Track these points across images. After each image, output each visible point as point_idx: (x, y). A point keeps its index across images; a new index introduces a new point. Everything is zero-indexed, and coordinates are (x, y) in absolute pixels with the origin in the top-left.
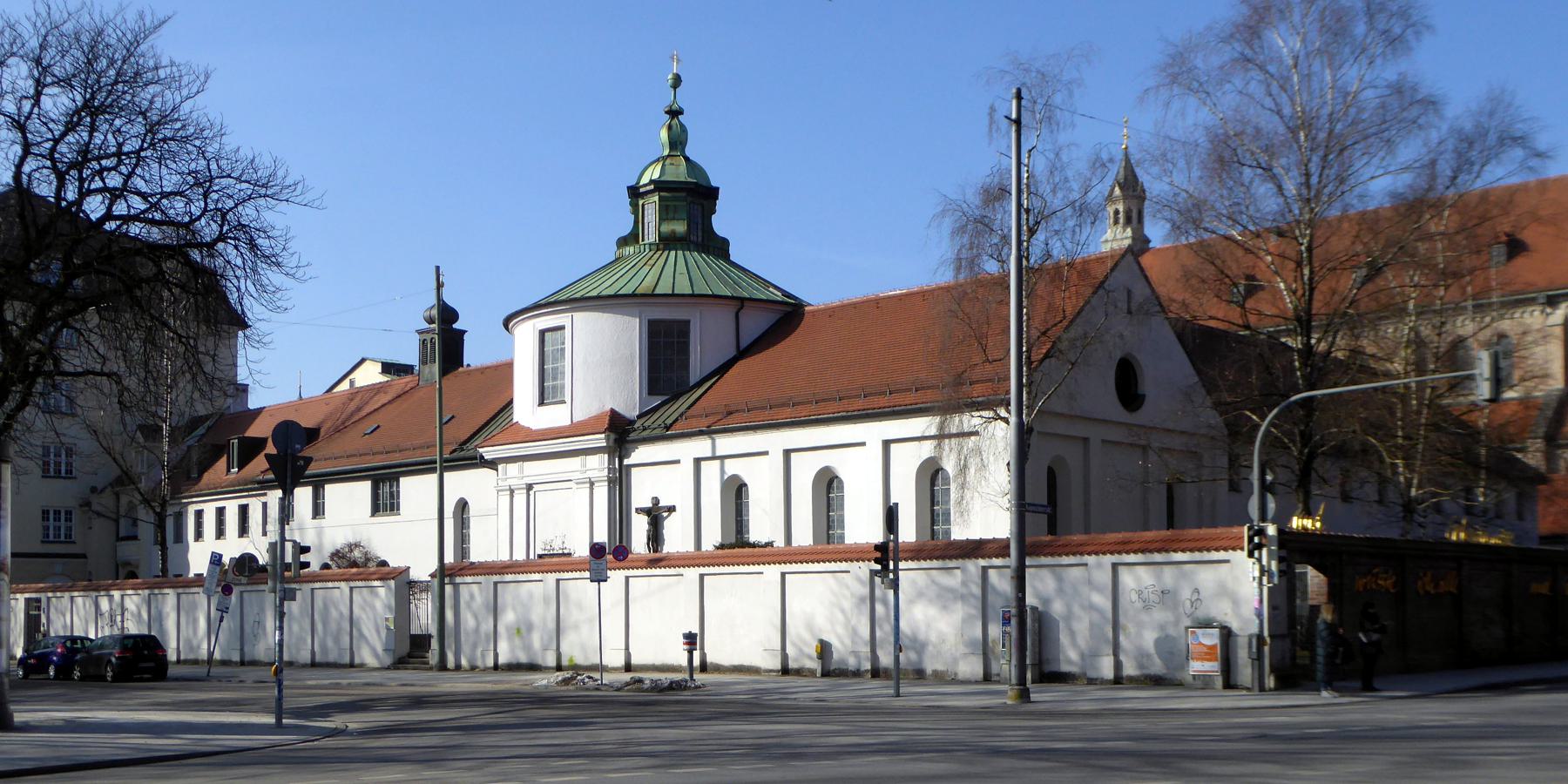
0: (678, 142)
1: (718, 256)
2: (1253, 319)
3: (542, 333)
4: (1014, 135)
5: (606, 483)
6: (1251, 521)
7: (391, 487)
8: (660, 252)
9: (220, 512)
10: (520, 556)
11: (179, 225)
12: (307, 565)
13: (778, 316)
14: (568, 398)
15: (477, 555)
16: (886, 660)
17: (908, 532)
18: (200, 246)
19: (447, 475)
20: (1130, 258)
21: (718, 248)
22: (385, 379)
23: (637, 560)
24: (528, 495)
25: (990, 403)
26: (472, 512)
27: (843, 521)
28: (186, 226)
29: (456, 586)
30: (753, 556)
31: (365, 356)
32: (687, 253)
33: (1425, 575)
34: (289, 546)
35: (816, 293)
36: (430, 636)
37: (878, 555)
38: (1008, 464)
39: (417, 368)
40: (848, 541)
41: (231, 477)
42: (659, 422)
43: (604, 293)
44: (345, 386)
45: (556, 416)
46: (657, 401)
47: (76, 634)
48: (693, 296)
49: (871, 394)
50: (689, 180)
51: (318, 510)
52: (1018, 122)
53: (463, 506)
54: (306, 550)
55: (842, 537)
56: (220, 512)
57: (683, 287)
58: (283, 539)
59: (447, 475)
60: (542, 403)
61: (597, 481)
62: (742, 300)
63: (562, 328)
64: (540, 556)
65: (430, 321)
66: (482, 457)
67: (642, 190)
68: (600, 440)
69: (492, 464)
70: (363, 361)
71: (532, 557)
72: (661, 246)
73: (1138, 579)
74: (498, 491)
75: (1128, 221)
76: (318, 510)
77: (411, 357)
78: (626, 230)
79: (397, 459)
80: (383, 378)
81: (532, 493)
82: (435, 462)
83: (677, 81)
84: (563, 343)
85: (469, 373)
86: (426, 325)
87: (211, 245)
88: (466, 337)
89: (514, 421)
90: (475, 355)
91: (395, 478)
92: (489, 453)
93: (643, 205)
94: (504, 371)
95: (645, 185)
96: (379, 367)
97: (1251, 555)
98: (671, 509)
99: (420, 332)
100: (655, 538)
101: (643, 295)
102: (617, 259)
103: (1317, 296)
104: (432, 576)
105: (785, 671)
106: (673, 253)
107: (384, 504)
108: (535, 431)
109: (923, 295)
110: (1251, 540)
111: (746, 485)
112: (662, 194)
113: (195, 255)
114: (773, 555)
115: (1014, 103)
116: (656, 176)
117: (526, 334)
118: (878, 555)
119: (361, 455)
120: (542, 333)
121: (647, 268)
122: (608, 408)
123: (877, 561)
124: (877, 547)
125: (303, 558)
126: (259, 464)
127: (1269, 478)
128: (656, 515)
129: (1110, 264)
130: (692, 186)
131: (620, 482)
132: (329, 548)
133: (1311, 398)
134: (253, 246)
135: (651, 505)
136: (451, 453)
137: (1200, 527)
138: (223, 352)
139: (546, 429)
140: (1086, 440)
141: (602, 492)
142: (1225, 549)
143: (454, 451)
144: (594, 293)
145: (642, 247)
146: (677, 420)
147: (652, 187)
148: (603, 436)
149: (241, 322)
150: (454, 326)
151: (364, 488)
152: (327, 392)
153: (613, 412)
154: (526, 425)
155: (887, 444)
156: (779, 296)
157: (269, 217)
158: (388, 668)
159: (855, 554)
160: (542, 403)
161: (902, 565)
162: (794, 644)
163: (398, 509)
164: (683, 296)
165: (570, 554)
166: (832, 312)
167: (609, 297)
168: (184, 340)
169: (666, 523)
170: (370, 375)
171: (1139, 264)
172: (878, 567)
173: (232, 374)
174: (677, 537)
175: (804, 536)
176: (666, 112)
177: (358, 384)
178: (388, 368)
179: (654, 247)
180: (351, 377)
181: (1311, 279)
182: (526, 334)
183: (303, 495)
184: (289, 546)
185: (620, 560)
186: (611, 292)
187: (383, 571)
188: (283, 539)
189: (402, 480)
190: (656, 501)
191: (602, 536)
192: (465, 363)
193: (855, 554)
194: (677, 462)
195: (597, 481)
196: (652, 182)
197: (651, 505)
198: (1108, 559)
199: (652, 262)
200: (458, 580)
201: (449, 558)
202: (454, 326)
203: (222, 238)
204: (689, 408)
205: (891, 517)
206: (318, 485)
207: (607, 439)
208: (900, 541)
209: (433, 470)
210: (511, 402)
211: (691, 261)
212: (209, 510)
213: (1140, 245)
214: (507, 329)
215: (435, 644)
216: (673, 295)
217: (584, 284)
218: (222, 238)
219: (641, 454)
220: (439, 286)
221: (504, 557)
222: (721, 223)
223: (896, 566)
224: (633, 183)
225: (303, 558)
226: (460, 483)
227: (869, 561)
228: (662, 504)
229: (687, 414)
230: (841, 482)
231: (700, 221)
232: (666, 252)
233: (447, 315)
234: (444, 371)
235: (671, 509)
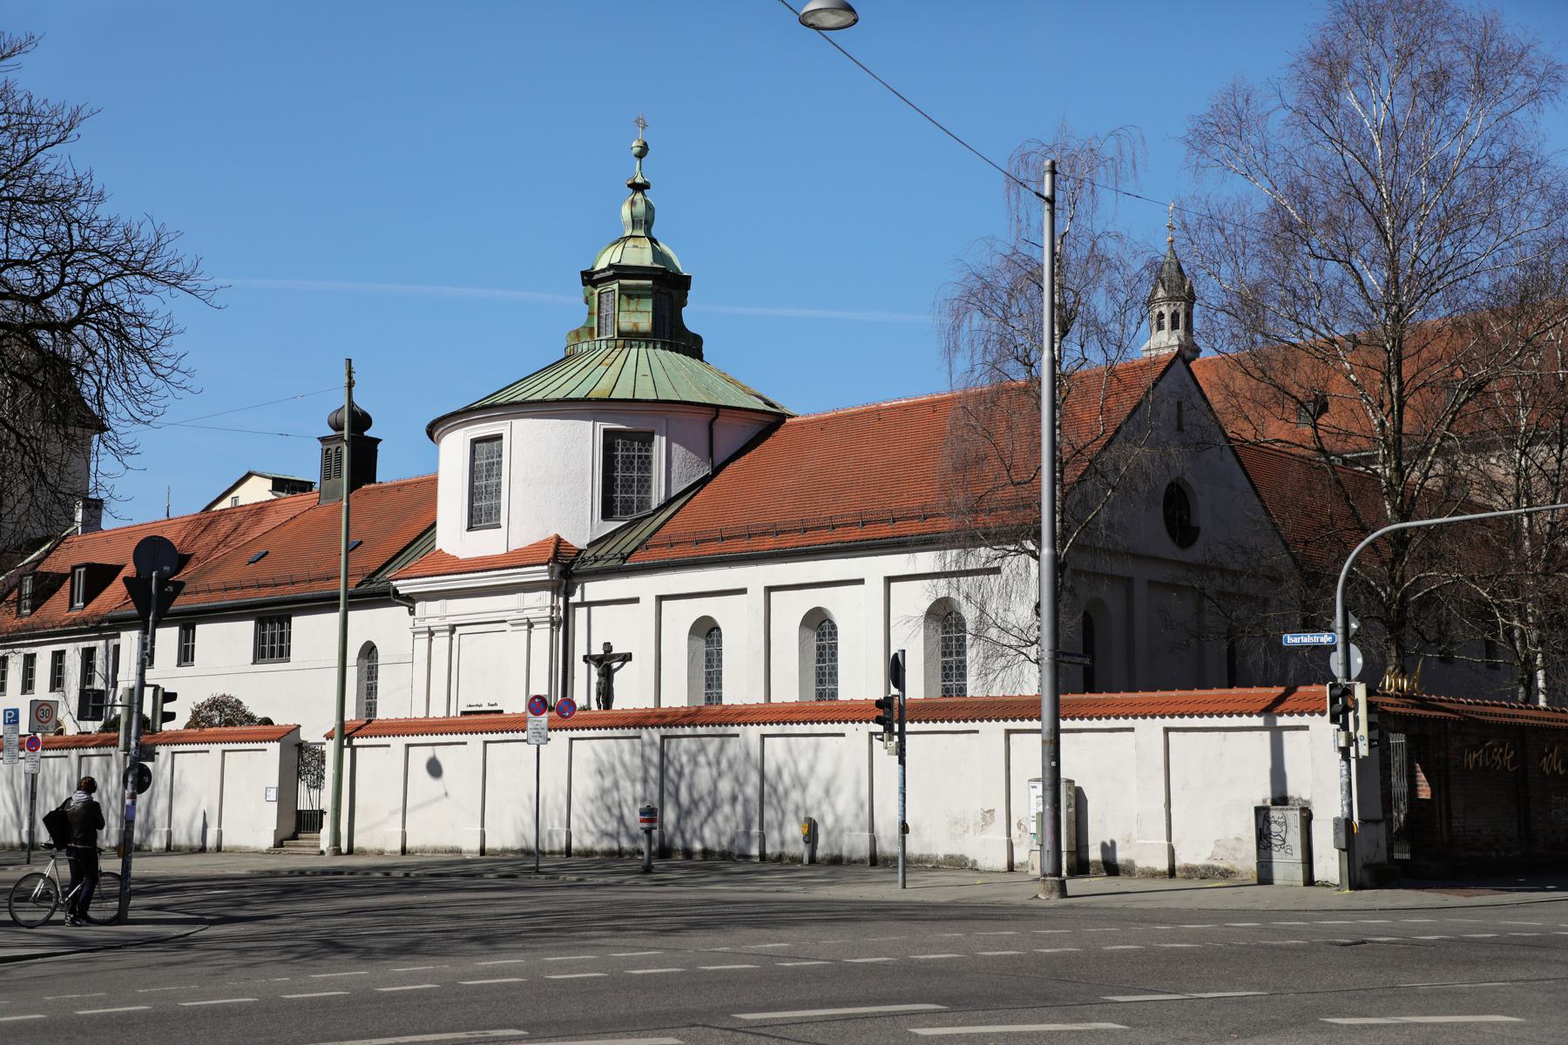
0: (645, 222)
2: (1328, 442)
3: (475, 442)
4: (1047, 216)
6: (1334, 678)
7: (282, 628)
9: (58, 657)
10: (438, 712)
11: (25, 300)
13: (761, 428)
14: (503, 522)
15: (384, 712)
16: (889, 845)
17: (916, 688)
18: (51, 327)
20: (1179, 362)
21: (691, 346)
23: (378, 728)
24: (451, 639)
25: (1018, 533)
26: (380, 660)
28: (37, 301)
29: (354, 749)
30: (1206, 702)
31: (252, 470)
32: (650, 350)
33: (1552, 750)
34: (148, 692)
35: (800, 404)
36: (322, 812)
37: (881, 713)
38: (1038, 606)
39: (317, 486)
41: (74, 614)
42: (615, 551)
43: (551, 397)
44: (226, 504)
45: (488, 543)
46: (613, 526)
49: (870, 522)
50: (656, 265)
51: (186, 655)
52: (1051, 201)
53: (369, 651)
54: (171, 697)
56: (58, 657)
57: (646, 392)
58: (142, 684)
59: (353, 615)
60: (470, 528)
61: (537, 623)
62: (717, 408)
63: (499, 437)
64: (464, 713)
66: (396, 592)
68: (541, 573)
69: (410, 600)
70: (249, 475)
71: (453, 713)
72: (620, 343)
73: (650, 735)
74: (415, 633)
75: (1174, 326)
76: (186, 655)
77: (309, 470)
78: (580, 320)
81: (455, 636)
82: (338, 598)
83: (643, 152)
84: (500, 456)
85: (384, 490)
86: (332, 432)
87: (67, 327)
88: (379, 447)
89: (437, 548)
90: (388, 470)
91: (285, 620)
92: (404, 587)
93: (599, 294)
94: (427, 489)
95: (603, 271)
96: (269, 484)
97: (1334, 720)
98: (627, 658)
99: (323, 440)
100: (606, 695)
101: (598, 400)
102: (567, 357)
103: (1408, 416)
104: (329, 736)
107: (272, 648)
109: (934, 405)
110: (1334, 700)
111: (718, 628)
113: (45, 337)
114: (504, 722)
115: (1048, 177)
117: (455, 447)
118: (881, 713)
120: (475, 442)
121: (602, 368)
122: (551, 534)
123: (879, 720)
124: (879, 704)
125: (168, 707)
126: (114, 596)
127: (1354, 626)
128: (607, 663)
129: (1161, 368)
130: (660, 273)
131: (563, 623)
133: (1404, 530)
134: (121, 334)
136: (357, 586)
137: (1231, 687)
138: (76, 462)
139: (476, 559)
140: (1130, 580)
141: (542, 635)
142: (1301, 714)
144: (538, 397)
145: (598, 344)
146: (636, 549)
148: (546, 567)
149: (99, 426)
150: (366, 433)
151: (247, 628)
154: (452, 553)
155: (889, 580)
156: (761, 406)
157: (148, 304)
159: (853, 712)
160: (470, 528)
161: (909, 727)
164: (647, 401)
165: (501, 712)
166: (823, 425)
167: (558, 401)
168: (23, 440)
169: (616, 675)
170: (257, 491)
171: (1190, 370)
172: (880, 728)
173: (84, 488)
174: (631, 692)
175: (788, 690)
176: (629, 186)
177: (241, 503)
178: (280, 485)
179: (612, 344)
180: (234, 494)
181: (1400, 392)
182: (455, 447)
183: (167, 638)
184: (148, 692)
186: (559, 395)
187: (264, 729)
188: (142, 684)
189: (294, 620)
191: (540, 688)
193: (853, 712)
195: (537, 623)
196: (611, 266)
197: (602, 652)
198: (1160, 723)
199: (608, 361)
201: (350, 715)
203: (81, 319)
204: (651, 536)
205: (896, 671)
206: (187, 623)
207: (551, 572)
208: (907, 697)
209: (335, 608)
210: (434, 525)
212: (44, 655)
213: (1186, 355)
214: (431, 437)
217: (526, 385)
218: (81, 319)
219: (594, 590)
220: (350, 385)
221: (419, 713)
222: (693, 317)
223: (902, 728)
225: (168, 707)
226: (367, 624)
227: (867, 722)
229: (649, 543)
230: (834, 627)
231: (667, 314)
232: (626, 350)
233: (360, 420)
234: (354, 485)
235: (627, 658)
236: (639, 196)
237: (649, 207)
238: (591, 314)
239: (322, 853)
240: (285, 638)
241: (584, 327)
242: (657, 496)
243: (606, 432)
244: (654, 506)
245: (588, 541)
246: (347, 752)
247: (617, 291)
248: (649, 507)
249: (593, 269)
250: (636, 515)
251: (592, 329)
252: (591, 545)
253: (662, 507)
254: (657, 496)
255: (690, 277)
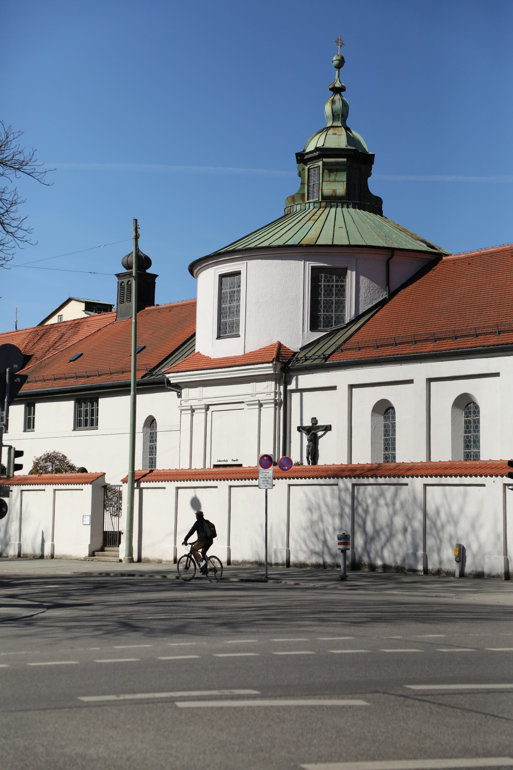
1: (376, 213)
5: (273, 405)
8: (322, 209)
12: (19, 467)
14: (242, 332)
15: (161, 465)
19: (138, 397)
22: (86, 316)
24: (206, 414)
27: (394, 444)
29: (141, 490)
31: (72, 296)
36: (120, 533)
39: (115, 307)
40: (398, 460)
42: (319, 353)
43: (275, 244)
44: (54, 320)
47: (115, 531)
48: (349, 246)
50: (349, 147)
53: (151, 422)
54: (19, 454)
55: (477, 456)
57: (341, 239)
59: (138, 397)
60: (219, 337)
62: (392, 250)
63: (238, 273)
64: (216, 466)
65: (128, 267)
66: (169, 382)
67: (306, 157)
68: (268, 369)
69: (178, 387)
70: (69, 300)
71: (208, 466)
74: (181, 410)
79: (97, 381)
80: (84, 315)
81: (209, 412)
84: (239, 286)
85: (160, 310)
86: (125, 271)
88: (157, 280)
89: (196, 351)
91: (94, 400)
92: (174, 378)
93: (309, 169)
96: (83, 306)
98: (328, 428)
99: (118, 276)
101: (308, 246)
104: (124, 481)
105: (288, 564)
106: (333, 210)
108: (215, 360)
111: (393, 408)
112: (325, 160)
114: (243, 473)
116: (320, 145)
119: (66, 378)
121: (311, 223)
122: (275, 341)
125: (18, 461)
130: (352, 153)
132: (40, 453)
135: (310, 425)
136: (143, 377)
139: (223, 359)
141: (269, 412)
143: (145, 376)
146: (334, 352)
147: (317, 153)
148: (271, 365)
150: (148, 271)
151: (69, 406)
152: (40, 325)
153: (280, 346)
154: (206, 355)
158: (118, 562)
162: (296, 541)
163: (34, 427)
165: (240, 465)
167: (279, 247)
169: (320, 441)
177: (64, 319)
178: (90, 307)
179: (317, 205)
180: (60, 313)
185: (285, 470)
186: (280, 242)
190: (314, 420)
191: (268, 449)
192: (156, 303)
194: (411, 382)
196: (317, 149)
197: (310, 425)
198: (227, 483)
199: (315, 218)
200: (143, 485)
201: (139, 466)
202: (148, 271)
204: (345, 342)
207: (275, 367)
209: (127, 392)
210: (194, 335)
211: (347, 217)
214: (192, 274)
215: (124, 539)
216: (333, 246)
217: (257, 236)
220: (137, 237)
224: (300, 150)
225: (18, 461)
227: (502, 476)
228: (319, 424)
230: (477, 407)
232: (327, 210)
234: (139, 308)
235: (328, 428)
236: (337, 97)
237: (345, 104)
238: (303, 184)
239: (121, 561)
240: (94, 413)
241: (298, 194)
242: (349, 314)
243: (313, 268)
244: (347, 320)
245: (300, 346)
246: (137, 492)
247: (321, 167)
248: (344, 322)
249: (304, 151)
250: (334, 328)
251: (303, 195)
252: (303, 349)
253: (349, 324)
254: (349, 314)
255: (373, 155)
